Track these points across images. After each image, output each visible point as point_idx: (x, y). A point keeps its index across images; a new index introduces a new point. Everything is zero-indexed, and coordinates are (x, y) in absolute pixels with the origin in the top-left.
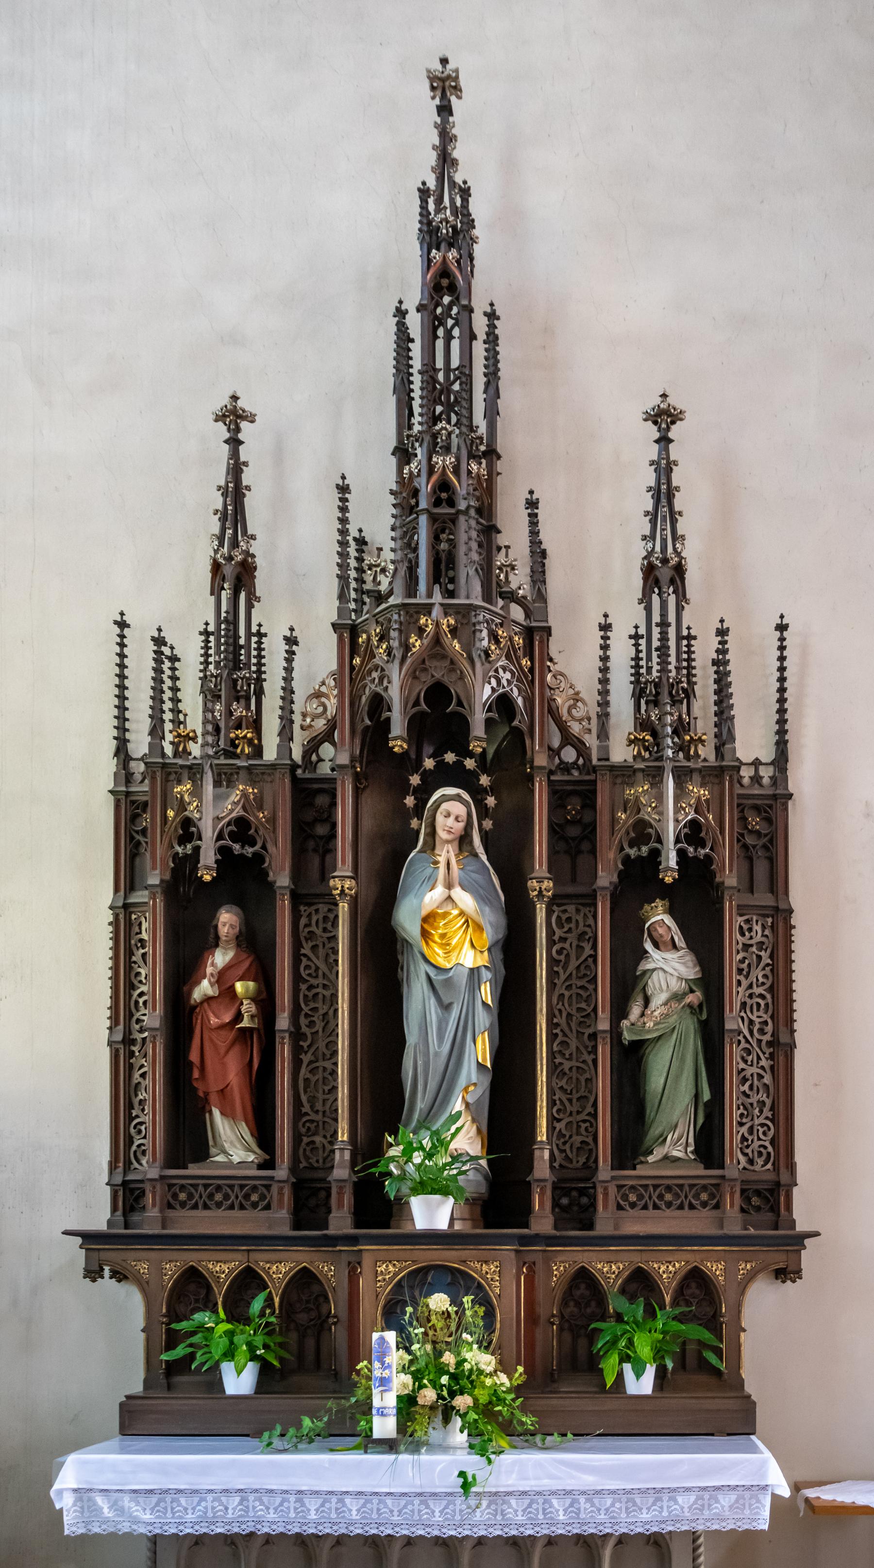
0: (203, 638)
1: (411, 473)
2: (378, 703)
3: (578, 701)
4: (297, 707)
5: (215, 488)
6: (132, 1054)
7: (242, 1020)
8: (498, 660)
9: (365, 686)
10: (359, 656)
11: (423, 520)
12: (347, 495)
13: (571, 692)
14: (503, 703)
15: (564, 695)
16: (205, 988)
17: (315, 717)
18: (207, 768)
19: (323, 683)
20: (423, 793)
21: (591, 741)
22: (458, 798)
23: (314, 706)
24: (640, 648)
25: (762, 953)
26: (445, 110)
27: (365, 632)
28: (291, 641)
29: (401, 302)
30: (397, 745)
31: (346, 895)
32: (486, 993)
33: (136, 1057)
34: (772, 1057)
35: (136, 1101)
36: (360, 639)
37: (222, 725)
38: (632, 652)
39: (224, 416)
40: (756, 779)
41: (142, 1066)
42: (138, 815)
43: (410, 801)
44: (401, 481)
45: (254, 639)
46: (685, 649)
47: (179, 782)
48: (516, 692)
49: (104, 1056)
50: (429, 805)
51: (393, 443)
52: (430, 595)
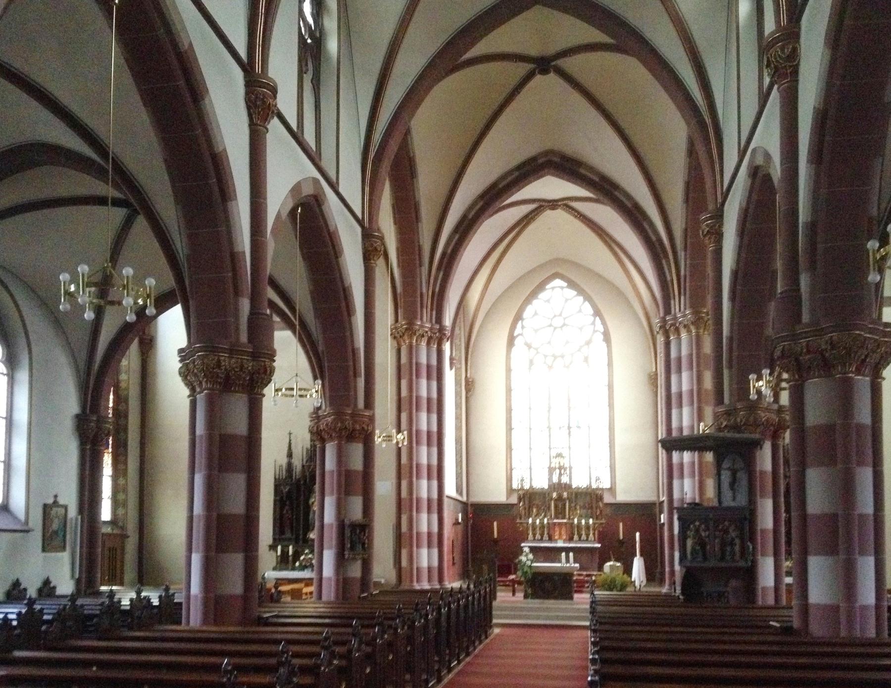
16: (285, 512)
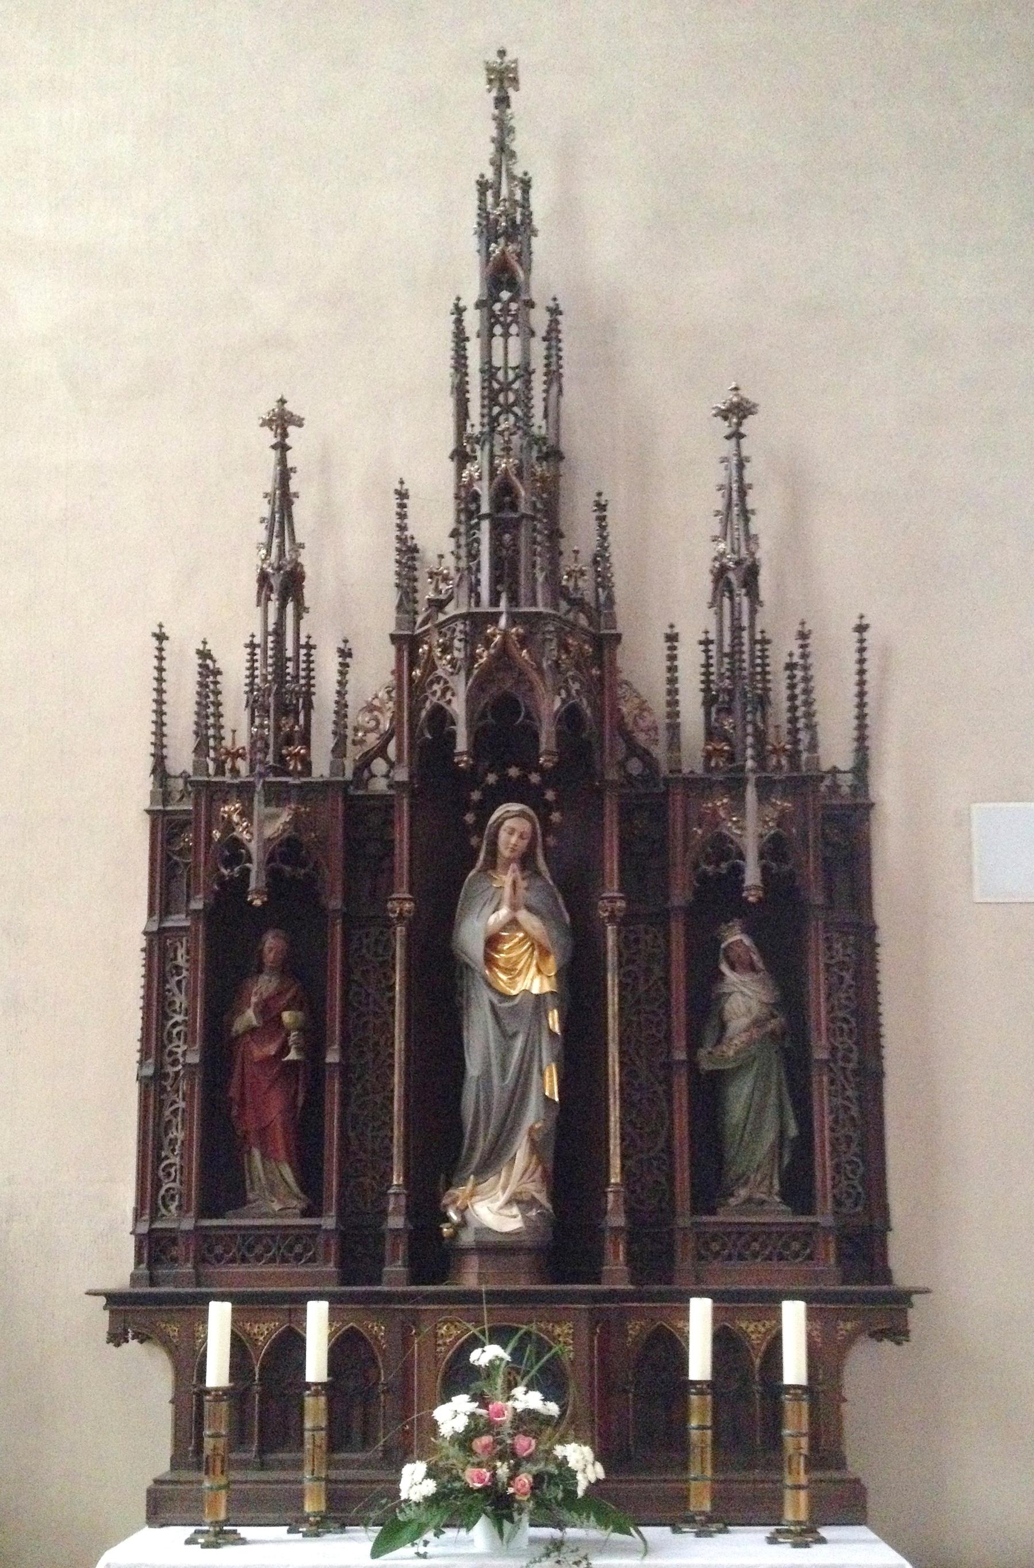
0: (249, 650)
1: (471, 476)
2: (441, 717)
3: (644, 710)
4: (350, 721)
5: (262, 495)
6: (163, 1090)
7: (289, 1052)
8: (568, 670)
9: (427, 698)
10: (419, 667)
11: (485, 525)
12: (405, 501)
13: (636, 701)
14: (570, 717)
15: (629, 704)
16: (250, 1016)
17: (367, 731)
18: (259, 787)
19: (376, 697)
20: (485, 809)
21: (660, 752)
22: (521, 814)
23: (367, 719)
24: (710, 654)
25: (844, 974)
26: (502, 101)
27: (426, 643)
28: (345, 654)
29: (458, 299)
30: (462, 761)
31: (404, 918)
32: (554, 1020)
33: (168, 1093)
34: (859, 1085)
35: (166, 1142)
36: (421, 650)
37: (271, 741)
38: (702, 659)
39: (270, 420)
40: (835, 788)
41: (174, 1102)
42: (176, 835)
43: (470, 818)
44: (459, 486)
45: (303, 651)
46: (759, 654)
47: (225, 802)
48: (585, 702)
49: (133, 1091)
50: (490, 822)
51: (450, 446)
52: (495, 601)
